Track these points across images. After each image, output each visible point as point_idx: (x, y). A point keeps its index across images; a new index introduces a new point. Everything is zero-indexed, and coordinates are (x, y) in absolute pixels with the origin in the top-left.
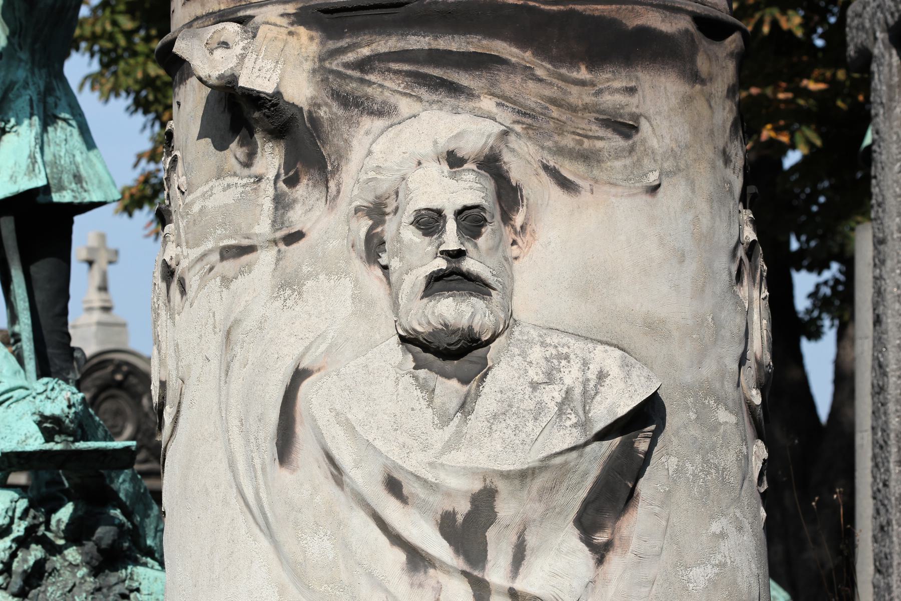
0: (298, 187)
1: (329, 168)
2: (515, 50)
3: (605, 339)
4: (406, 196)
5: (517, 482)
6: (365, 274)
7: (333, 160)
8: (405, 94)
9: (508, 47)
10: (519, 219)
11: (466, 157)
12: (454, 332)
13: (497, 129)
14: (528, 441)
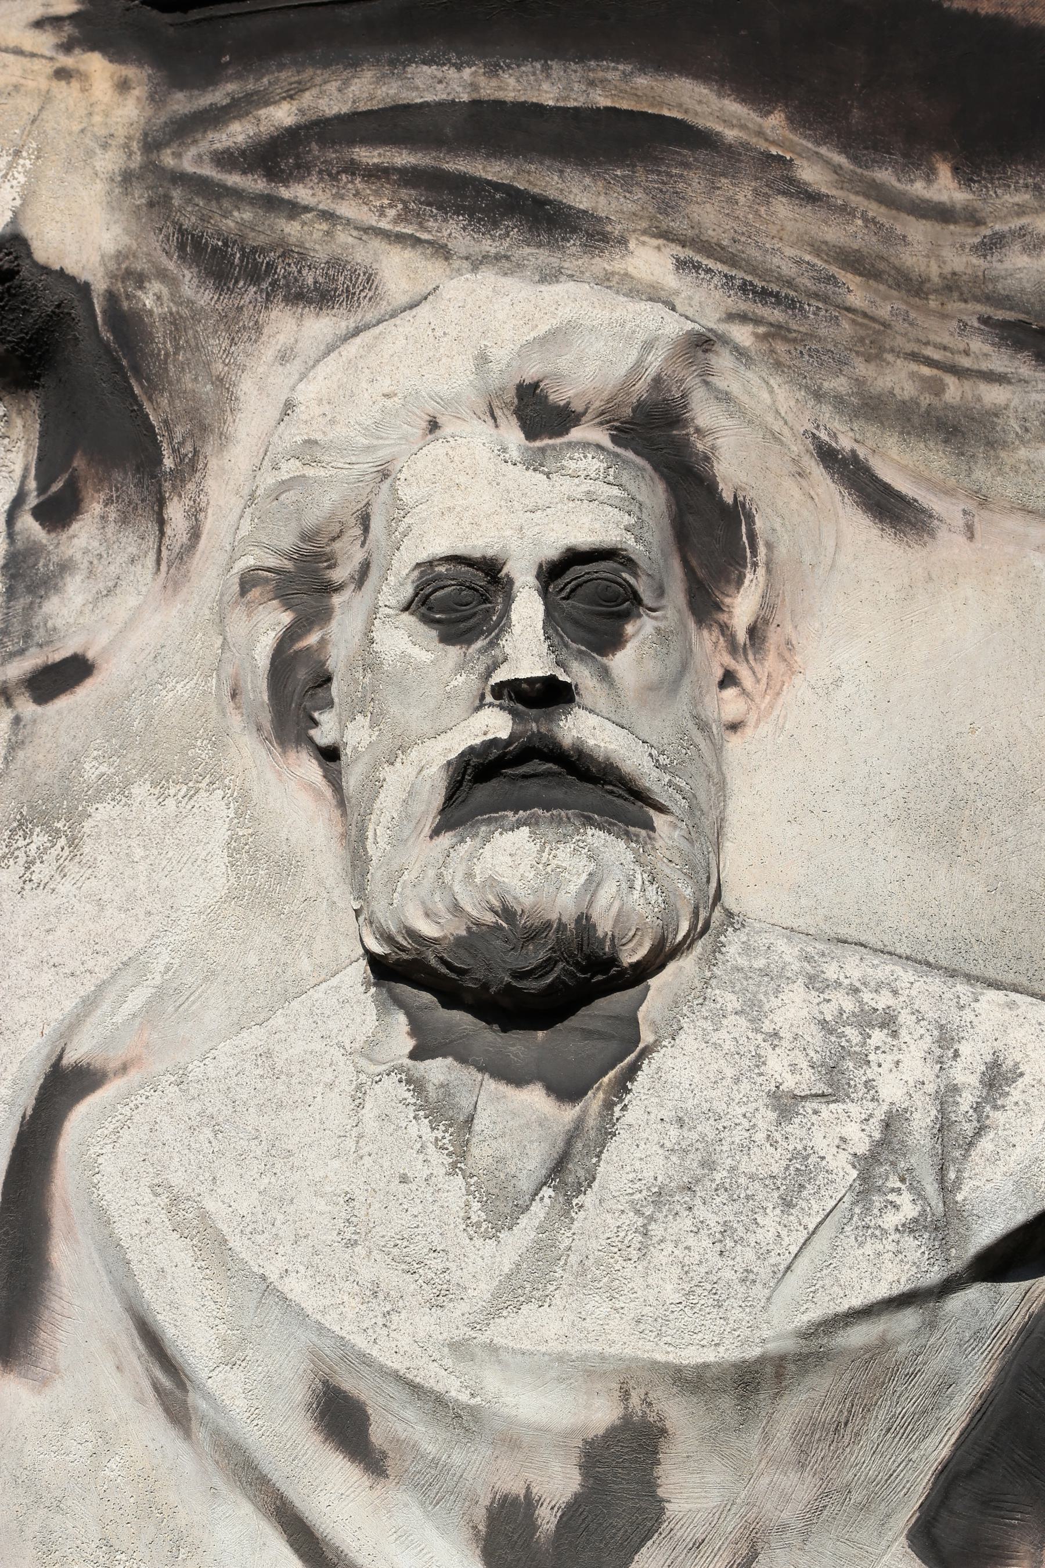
0: (75, 526)
1: (168, 463)
2: (734, 107)
3: (1010, 978)
4: (392, 521)
5: (726, 1402)
6: (270, 776)
7: (178, 438)
8: (400, 239)
9: (713, 97)
10: (742, 607)
11: (578, 406)
12: (534, 934)
13: (673, 327)
14: (764, 1272)
